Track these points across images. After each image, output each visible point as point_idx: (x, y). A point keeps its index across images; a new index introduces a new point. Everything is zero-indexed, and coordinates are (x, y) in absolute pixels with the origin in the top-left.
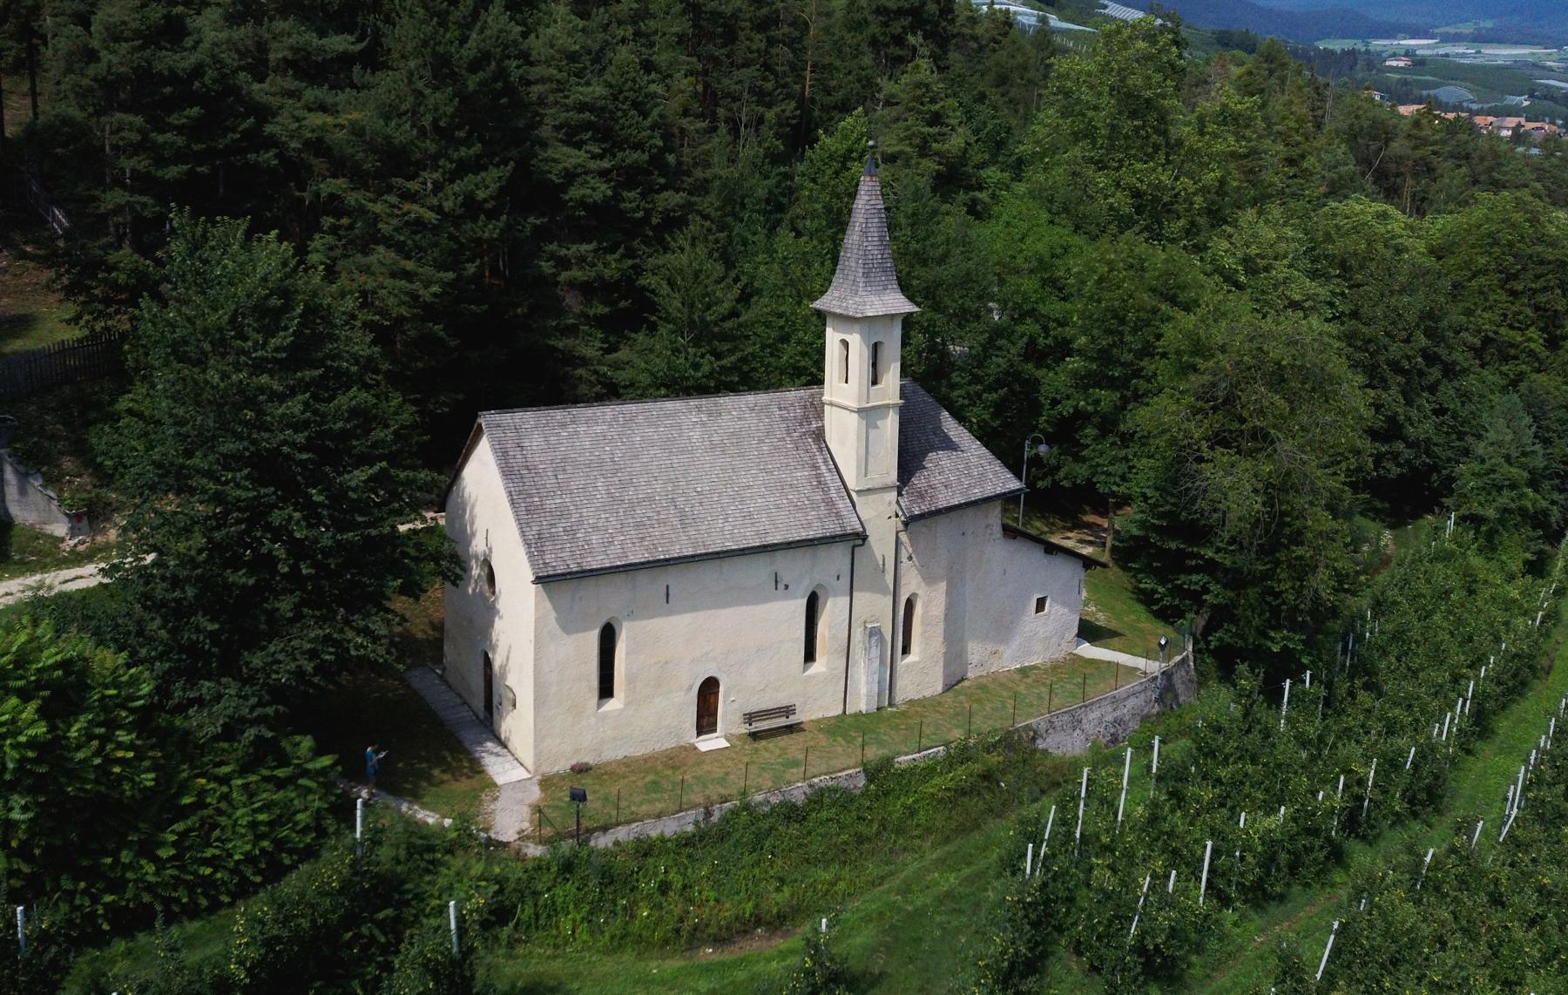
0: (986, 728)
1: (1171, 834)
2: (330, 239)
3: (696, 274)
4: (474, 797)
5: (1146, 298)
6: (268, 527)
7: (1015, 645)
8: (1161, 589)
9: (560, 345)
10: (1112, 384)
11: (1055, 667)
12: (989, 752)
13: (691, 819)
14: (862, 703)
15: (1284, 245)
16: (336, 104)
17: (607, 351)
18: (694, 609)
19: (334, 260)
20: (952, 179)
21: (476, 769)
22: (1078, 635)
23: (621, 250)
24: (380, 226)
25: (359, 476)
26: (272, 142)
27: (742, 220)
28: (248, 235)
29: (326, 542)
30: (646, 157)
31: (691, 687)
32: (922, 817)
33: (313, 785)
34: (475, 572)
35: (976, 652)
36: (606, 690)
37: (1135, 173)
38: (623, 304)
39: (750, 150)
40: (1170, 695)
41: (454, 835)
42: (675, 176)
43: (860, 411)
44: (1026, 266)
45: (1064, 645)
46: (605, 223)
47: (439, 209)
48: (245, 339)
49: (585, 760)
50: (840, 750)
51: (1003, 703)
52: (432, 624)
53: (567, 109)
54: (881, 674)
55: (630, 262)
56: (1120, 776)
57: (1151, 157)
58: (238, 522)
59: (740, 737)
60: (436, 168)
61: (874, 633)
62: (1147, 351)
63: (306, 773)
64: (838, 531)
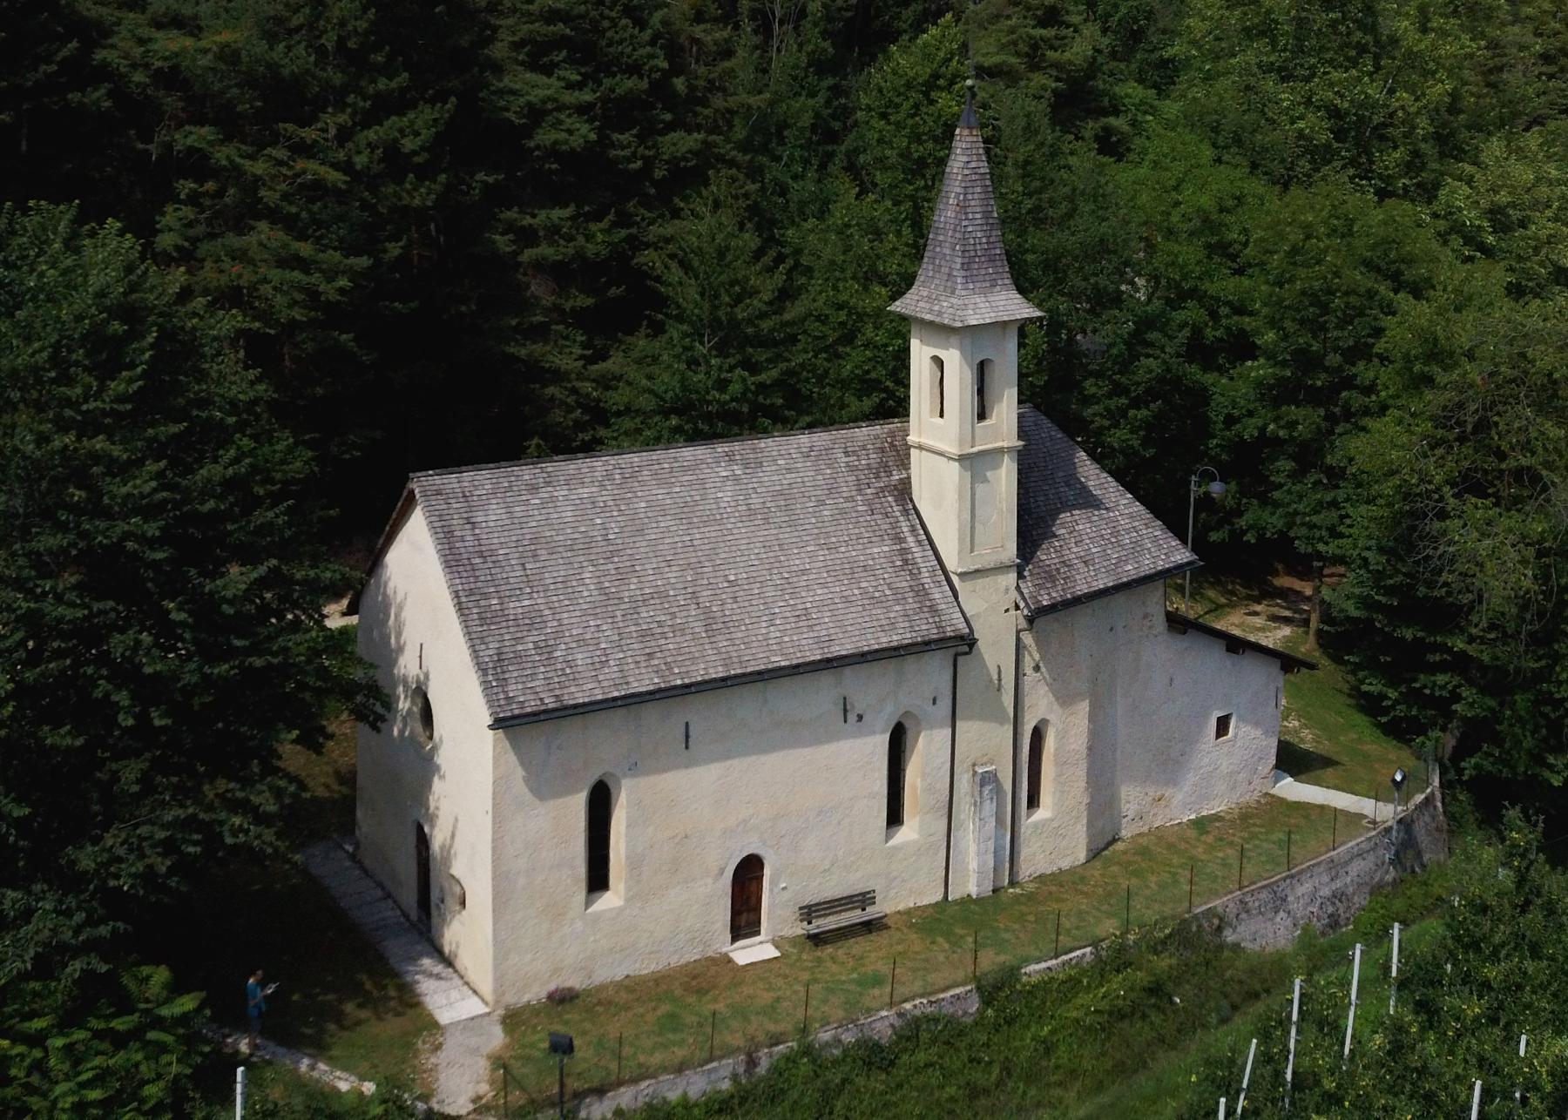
0: (1151, 916)
1: (1422, 1071)
2: (188, 212)
3: (721, 254)
4: (407, 1045)
5: (1359, 278)
6: (104, 659)
7: (1190, 779)
8: (1393, 694)
9: (523, 352)
10: (1316, 398)
11: (1245, 816)
12: (1156, 952)
13: (726, 1072)
14: (972, 881)
15: (1544, 189)
16: (196, 17)
17: (590, 360)
18: (727, 756)
19: (195, 241)
20: (1076, 100)
21: (409, 1001)
22: (1278, 766)
23: (611, 217)
24: (262, 193)
25: (237, 577)
26: (105, 73)
27: (778, 159)
28: (79, 221)
29: (189, 678)
30: (645, 84)
31: (722, 871)
32: (1062, 1054)
33: (168, 1039)
34: (403, 705)
35: (1132, 799)
36: (598, 880)
37: (1332, 85)
38: (614, 291)
39: (788, 55)
40: (1410, 854)
41: (379, 1110)
42: (684, 112)
43: (962, 459)
44: (1185, 227)
45: (1256, 781)
46: (589, 179)
47: (347, 167)
48: (70, 381)
49: (568, 984)
50: (941, 958)
51: (1174, 875)
52: (337, 773)
53: (530, 17)
54: (998, 838)
55: (624, 233)
56: (1345, 983)
57: (1354, 63)
58: (59, 654)
59: (794, 941)
60: (341, 106)
61: (988, 780)
62: (1360, 352)
63: (159, 1023)
64: (934, 634)
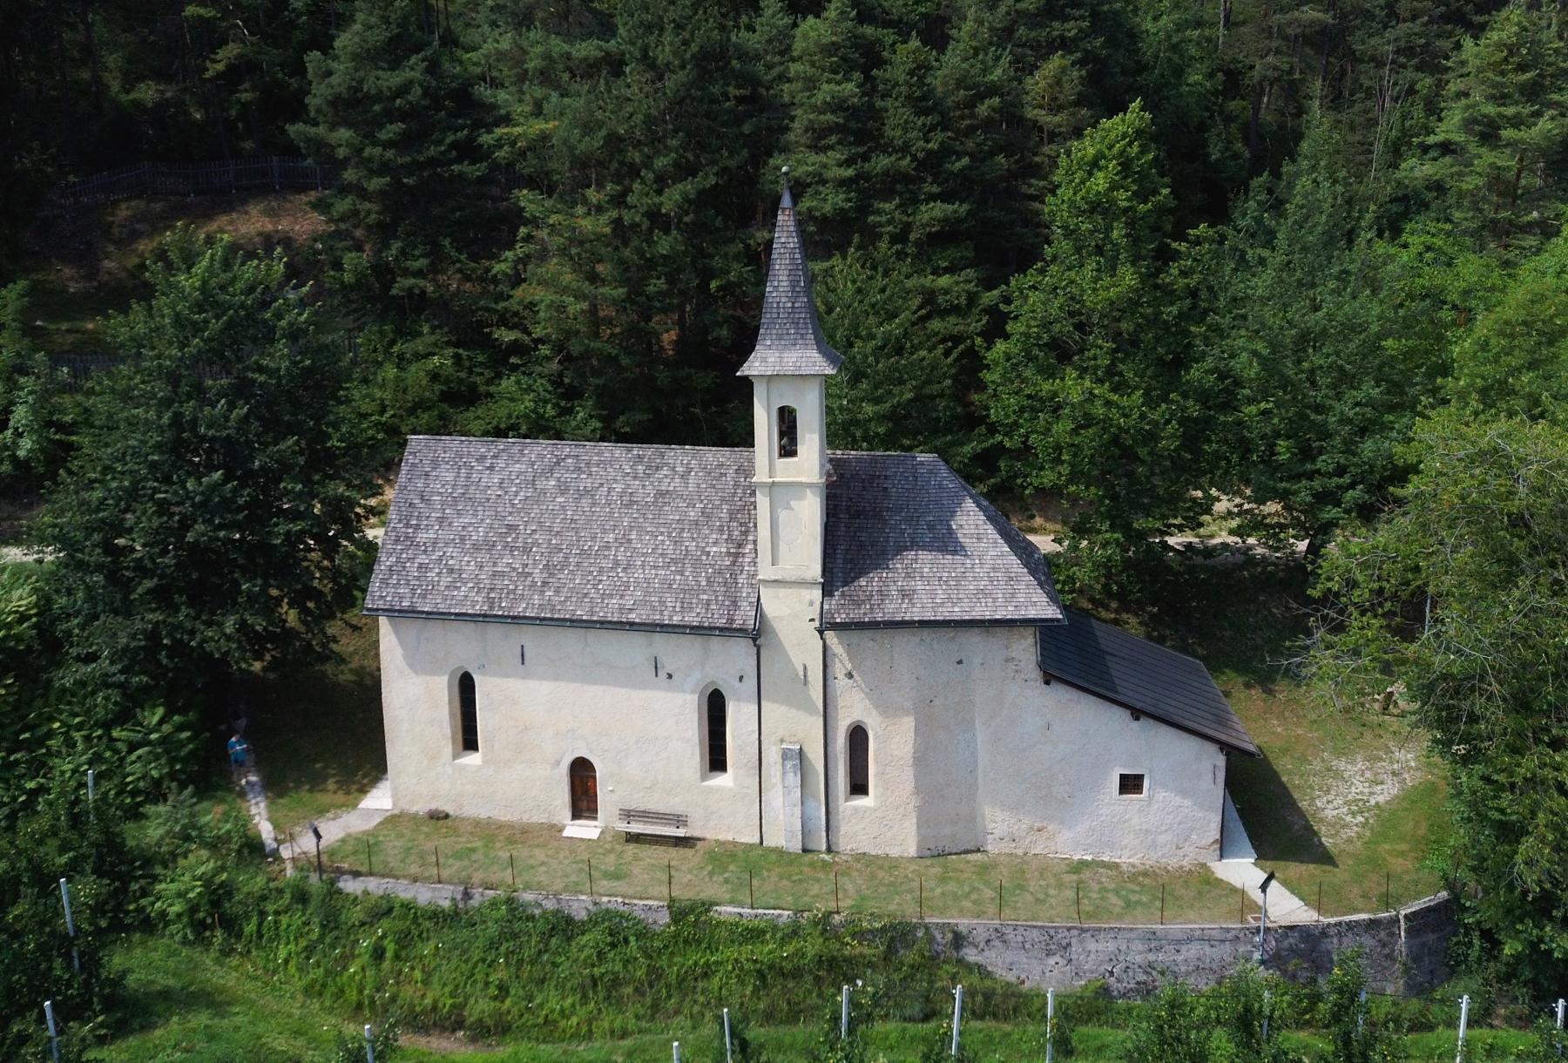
18: (557, 678)
31: (558, 763)
